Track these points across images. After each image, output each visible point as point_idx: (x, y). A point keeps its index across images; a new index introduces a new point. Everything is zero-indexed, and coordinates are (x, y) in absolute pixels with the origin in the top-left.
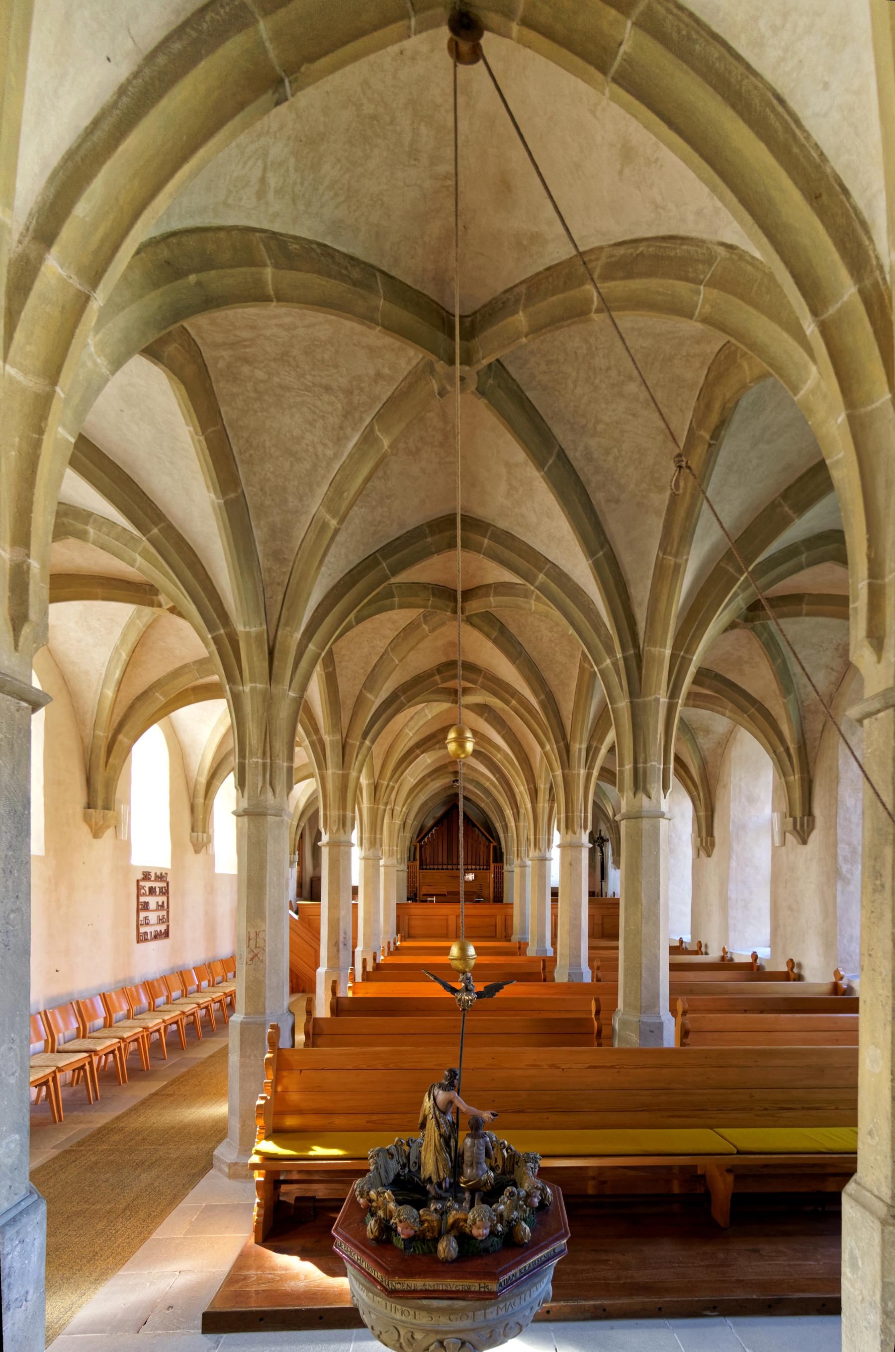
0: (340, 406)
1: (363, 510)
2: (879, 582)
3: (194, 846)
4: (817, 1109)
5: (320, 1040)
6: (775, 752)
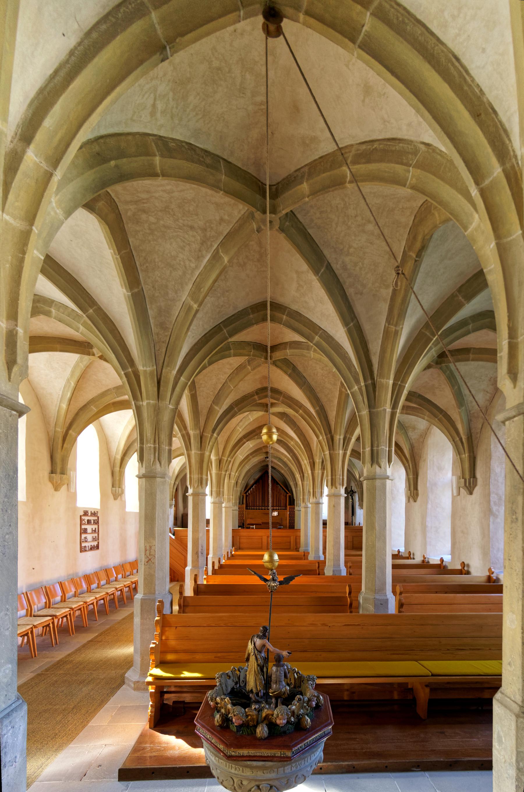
0: (199, 238)
1: (213, 299)
2: (515, 341)
3: (113, 496)
4: (479, 649)
5: (187, 609)
6: (453, 440)
